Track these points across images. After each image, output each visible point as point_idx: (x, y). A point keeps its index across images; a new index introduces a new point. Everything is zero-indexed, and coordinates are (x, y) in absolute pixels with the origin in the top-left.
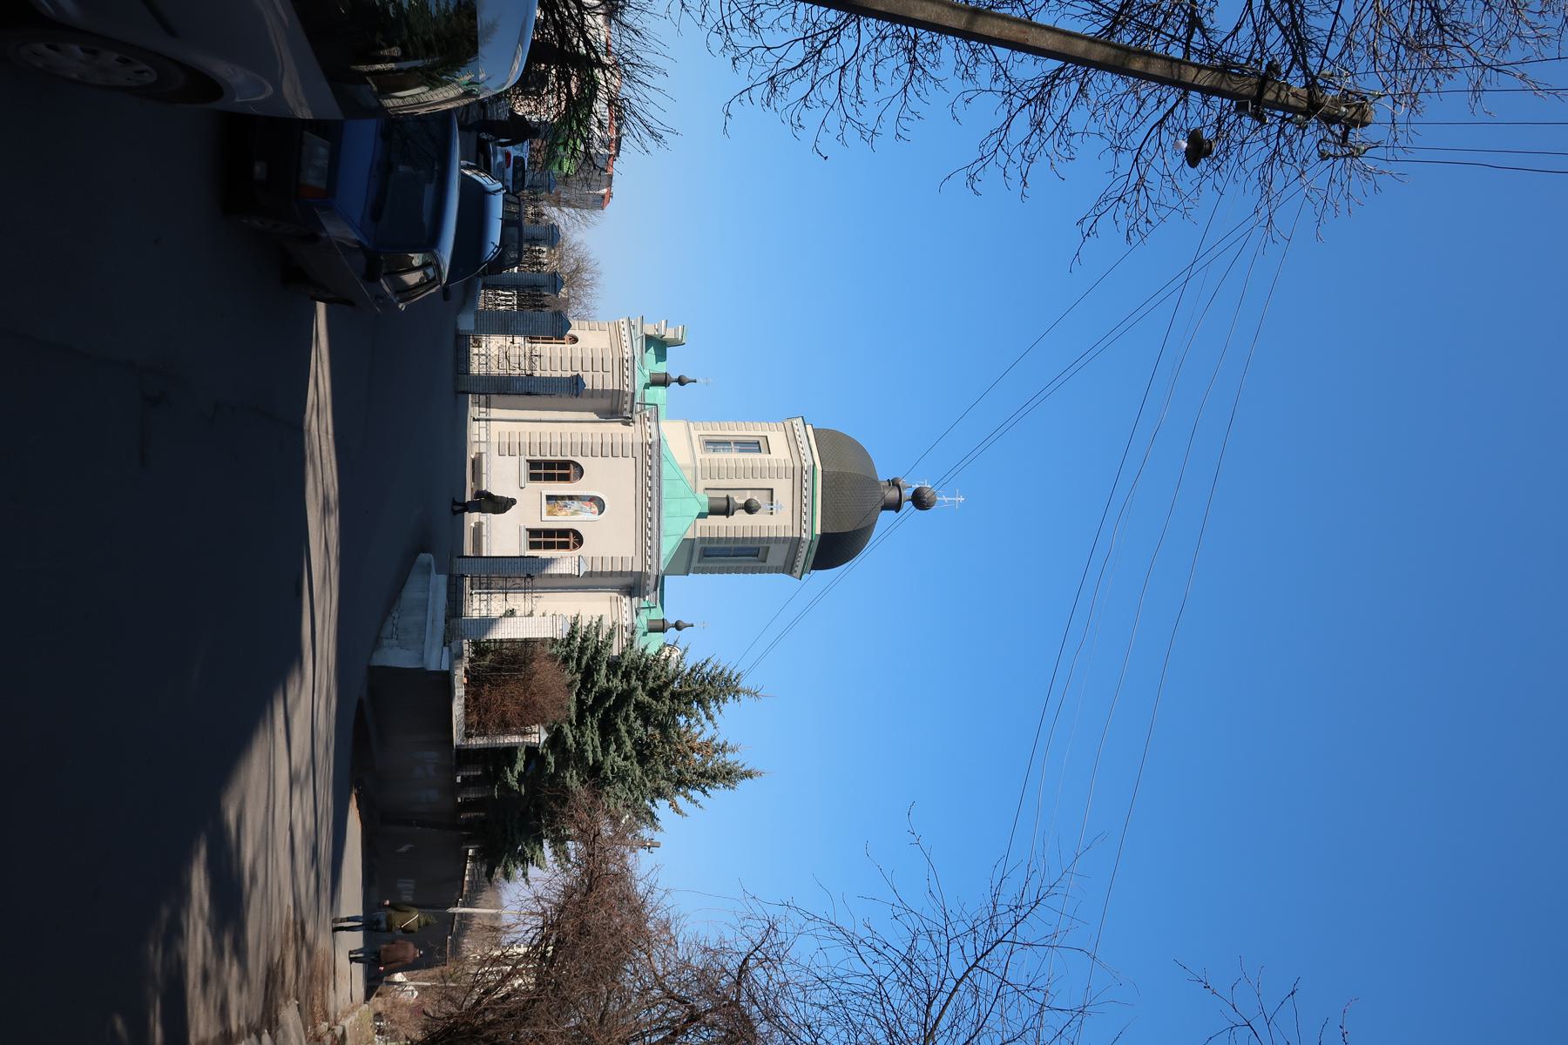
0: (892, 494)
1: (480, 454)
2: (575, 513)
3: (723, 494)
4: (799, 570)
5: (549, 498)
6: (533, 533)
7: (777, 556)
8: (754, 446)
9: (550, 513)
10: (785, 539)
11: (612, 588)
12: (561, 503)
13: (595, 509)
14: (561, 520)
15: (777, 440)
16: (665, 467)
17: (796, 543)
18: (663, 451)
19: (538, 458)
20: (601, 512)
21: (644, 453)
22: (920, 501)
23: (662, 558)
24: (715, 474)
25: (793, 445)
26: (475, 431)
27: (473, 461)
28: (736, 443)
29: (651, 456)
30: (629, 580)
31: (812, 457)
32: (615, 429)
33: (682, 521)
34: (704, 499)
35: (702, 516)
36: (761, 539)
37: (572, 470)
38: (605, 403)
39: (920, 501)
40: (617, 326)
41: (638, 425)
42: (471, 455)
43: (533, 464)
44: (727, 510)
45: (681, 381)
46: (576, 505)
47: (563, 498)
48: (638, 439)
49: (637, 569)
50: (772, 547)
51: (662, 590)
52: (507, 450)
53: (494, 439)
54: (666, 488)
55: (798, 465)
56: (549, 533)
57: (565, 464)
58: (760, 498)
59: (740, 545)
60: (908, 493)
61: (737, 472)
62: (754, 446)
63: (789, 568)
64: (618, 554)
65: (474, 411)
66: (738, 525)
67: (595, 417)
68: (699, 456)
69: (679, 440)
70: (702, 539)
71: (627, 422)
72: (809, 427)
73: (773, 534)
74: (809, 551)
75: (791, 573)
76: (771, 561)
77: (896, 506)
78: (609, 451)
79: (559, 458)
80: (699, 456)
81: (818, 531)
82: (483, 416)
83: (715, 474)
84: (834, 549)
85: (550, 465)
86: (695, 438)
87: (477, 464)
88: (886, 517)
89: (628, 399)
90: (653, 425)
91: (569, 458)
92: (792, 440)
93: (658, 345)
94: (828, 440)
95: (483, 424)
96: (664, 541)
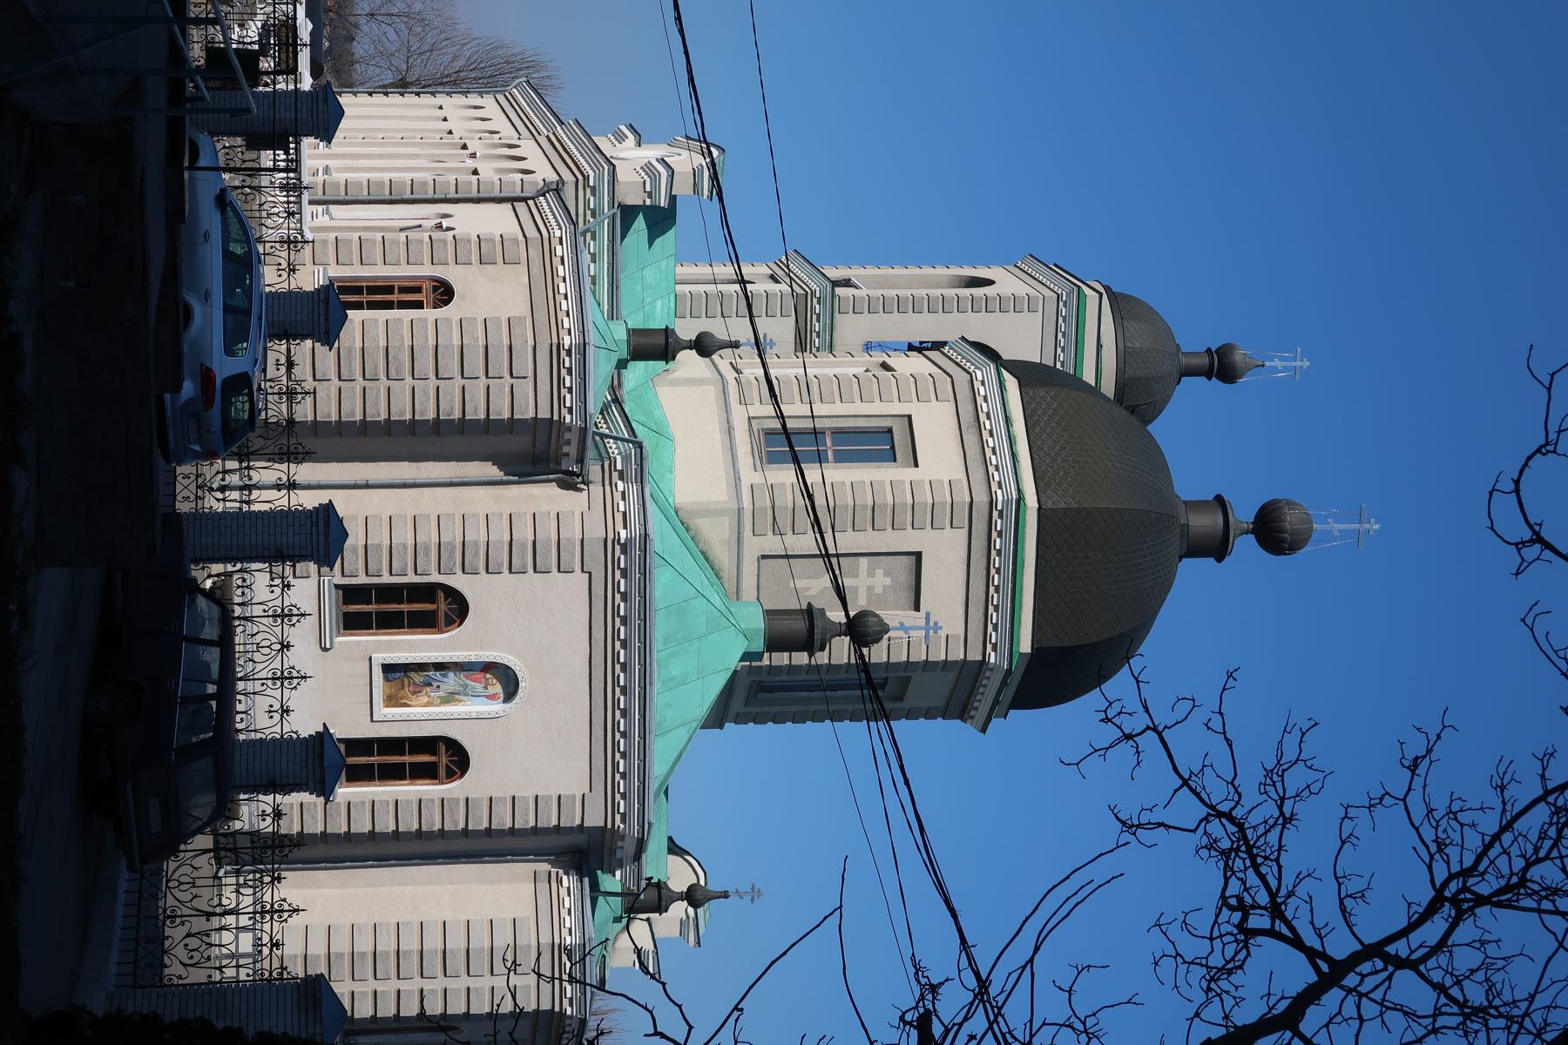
2: (450, 698)
4: (983, 706)
5: (388, 669)
9: (392, 701)
10: (946, 664)
11: (538, 854)
12: (418, 678)
13: (497, 688)
14: (419, 717)
15: (936, 428)
19: (362, 579)
21: (609, 563)
25: (971, 440)
32: (544, 497)
38: (521, 443)
39: (1272, 531)
41: (596, 489)
43: (350, 594)
46: (452, 681)
47: (421, 667)
48: (596, 531)
49: (595, 819)
50: (917, 678)
51: (721, 199)
55: (981, 498)
57: (427, 592)
64: (549, 791)
68: (750, 476)
71: (571, 481)
74: (1004, 683)
76: (911, 700)
77: (1218, 549)
78: (529, 557)
79: (411, 578)
81: (1025, 645)
88: (1192, 572)
89: (573, 436)
90: (633, 491)
92: (971, 426)
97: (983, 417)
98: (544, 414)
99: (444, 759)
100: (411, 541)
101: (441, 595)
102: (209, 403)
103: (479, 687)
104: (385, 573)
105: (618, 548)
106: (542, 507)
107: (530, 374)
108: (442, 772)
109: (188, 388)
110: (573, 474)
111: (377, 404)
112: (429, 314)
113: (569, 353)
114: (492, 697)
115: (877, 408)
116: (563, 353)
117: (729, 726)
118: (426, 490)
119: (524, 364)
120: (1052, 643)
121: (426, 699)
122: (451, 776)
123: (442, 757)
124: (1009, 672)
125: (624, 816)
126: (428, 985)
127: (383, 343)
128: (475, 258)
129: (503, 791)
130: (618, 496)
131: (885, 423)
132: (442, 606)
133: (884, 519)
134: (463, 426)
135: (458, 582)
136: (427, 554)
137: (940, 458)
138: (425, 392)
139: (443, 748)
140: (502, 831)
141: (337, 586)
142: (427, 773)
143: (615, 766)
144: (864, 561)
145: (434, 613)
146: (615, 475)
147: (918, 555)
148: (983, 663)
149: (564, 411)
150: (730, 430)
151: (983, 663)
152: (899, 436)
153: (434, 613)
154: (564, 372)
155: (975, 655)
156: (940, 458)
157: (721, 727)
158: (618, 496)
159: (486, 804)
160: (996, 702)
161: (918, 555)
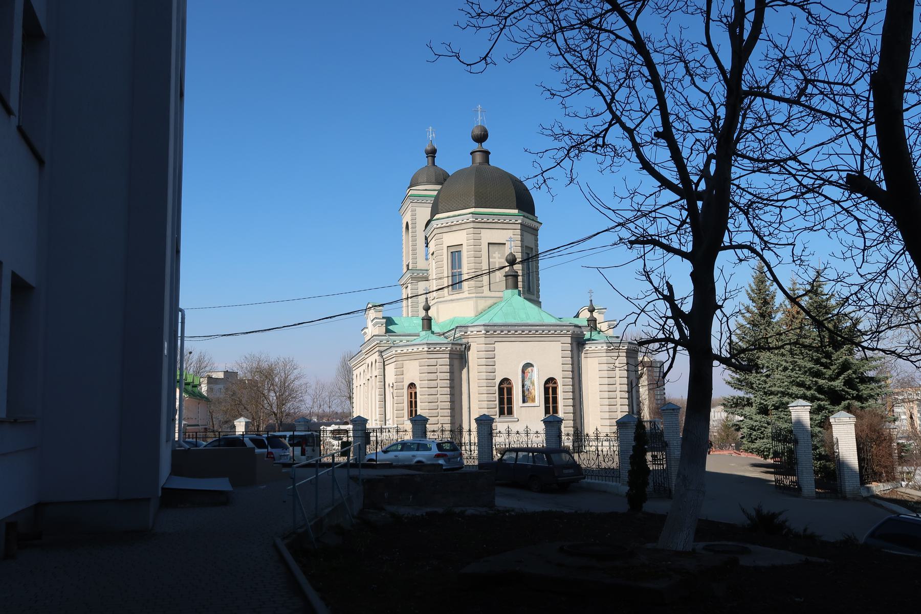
0: (479, 158)
2: (533, 383)
5: (524, 402)
7: (530, 242)
9: (533, 400)
11: (579, 356)
12: (526, 393)
13: (530, 369)
15: (451, 239)
20: (532, 365)
21: (492, 336)
30: (575, 344)
37: (505, 386)
38: (456, 362)
41: (470, 340)
43: (502, 413)
44: (33, 34)
45: (427, 308)
46: (527, 383)
47: (523, 392)
48: (483, 340)
49: (569, 340)
50: (526, 244)
54: (511, 321)
55: (472, 225)
57: (501, 390)
60: (476, 146)
63: (534, 231)
64: (560, 353)
68: (466, 295)
71: (468, 348)
75: (537, 230)
77: (486, 153)
78: (490, 360)
80: (466, 295)
81: (516, 211)
85: (501, 401)
88: (493, 162)
89: (454, 347)
90: (470, 329)
91: (497, 388)
92: (450, 228)
98: (448, 356)
99: (551, 385)
102: (445, 455)
109: (441, 462)
112: (418, 390)
119: (433, 362)
120: (515, 203)
122: (555, 383)
123: (550, 386)
126: (618, 389)
129: (560, 367)
133: (478, 254)
134: (452, 380)
135: (498, 381)
137: (460, 237)
142: (555, 390)
147: (489, 244)
156: (460, 237)
161: (489, 244)
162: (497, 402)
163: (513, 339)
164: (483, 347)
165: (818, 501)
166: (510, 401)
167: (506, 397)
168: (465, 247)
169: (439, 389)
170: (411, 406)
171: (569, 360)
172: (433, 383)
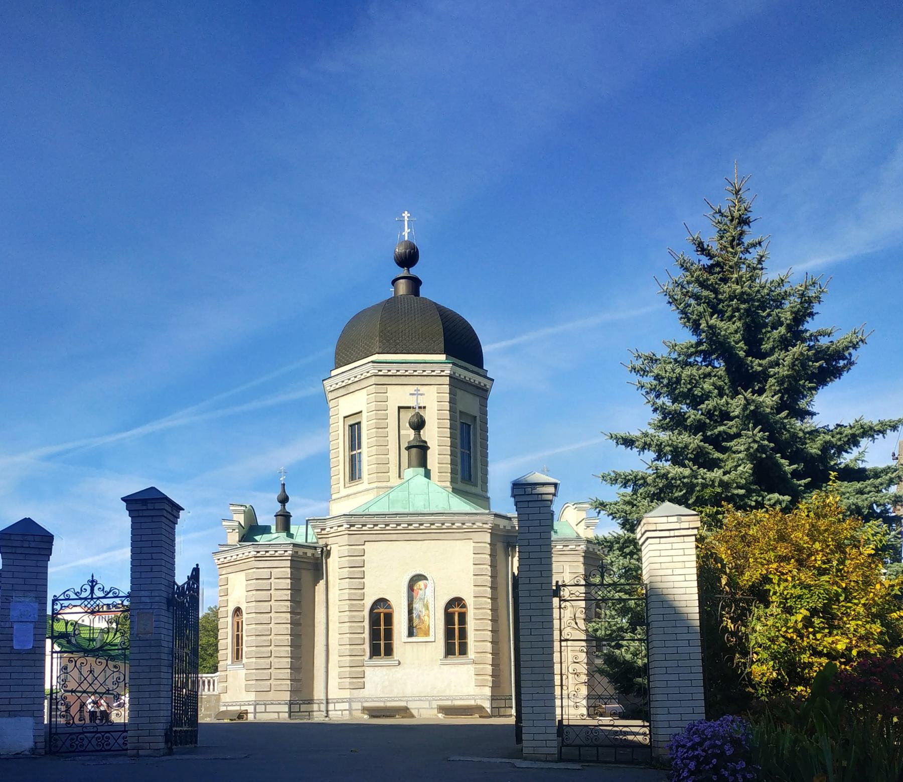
1: (365, 710)
3: (405, 453)
5: (411, 634)
6: (449, 651)
7: (469, 404)
8: (354, 431)
9: (427, 634)
12: (416, 622)
13: (421, 584)
15: (345, 406)
16: (374, 510)
17: (455, 383)
18: (360, 511)
19: (367, 647)
20: (425, 578)
21: (360, 532)
22: (409, 258)
23: (475, 511)
24: (383, 468)
26: (339, 714)
27: (373, 716)
28: (352, 448)
29: (358, 523)
30: (500, 547)
31: (363, 367)
32: (334, 565)
33: (433, 492)
34: (408, 473)
35: (428, 475)
36: (452, 419)
37: (382, 610)
38: (307, 576)
39: (409, 258)
40: (223, 565)
41: (330, 541)
42: (365, 719)
43: (375, 652)
44: (420, 451)
45: (284, 500)
46: (417, 606)
47: (410, 620)
50: (460, 407)
52: (357, 681)
53: (346, 694)
55: (373, 380)
56: (449, 634)
58: (407, 416)
59: (458, 441)
60: (403, 272)
61: (382, 445)
62: (354, 431)
63: (482, 393)
65: (318, 717)
66: (437, 436)
67: (322, 583)
69: (348, 499)
70: (453, 481)
72: (334, 373)
73: (447, 405)
76: (475, 411)
77: (415, 283)
78: (357, 571)
79: (366, 624)
81: (442, 357)
82: (323, 707)
83: (383, 468)
84: (462, 345)
85: (374, 635)
86: (344, 492)
87: (374, 712)
88: (424, 292)
92: (346, 389)
93: (251, 531)
94: (346, 352)
95: (331, 707)
96: (455, 509)
97: (344, 384)
98: (288, 564)
100: (348, 624)
101: (450, 610)
103: (421, 592)
104: (362, 636)
105: (352, 528)
106: (337, 565)
107: (269, 570)
108: (463, 610)
110: (322, 551)
111: (282, 640)
113: (258, 552)
114: (426, 587)
115: (341, 432)
116: (259, 555)
117: (489, 495)
118: (330, 619)
119: (265, 573)
120: (442, 345)
121: (426, 618)
122: (464, 606)
124: (454, 364)
125: (409, 525)
127: (254, 638)
128: (224, 598)
130: (332, 530)
131: (347, 428)
132: (382, 610)
133: (383, 423)
135: (368, 603)
136: (354, 617)
137: (356, 402)
138: (277, 618)
139: (450, 610)
140: (492, 582)
141: (371, 658)
142: (463, 617)
143: (459, 528)
144: (402, 432)
145: (385, 614)
146: (323, 532)
147: (400, 408)
148: (450, 377)
149: (286, 554)
150: (348, 496)
151: (450, 377)
152: (352, 421)
153: (385, 614)
154: (267, 554)
155: (447, 380)
156: (356, 402)
157: (488, 498)
158: (332, 530)
159: (477, 588)
160: (478, 374)
161: (400, 408)
162: (366, 635)
163: (394, 537)
164: (345, 550)
165: (561, 765)
166: (389, 634)
167: (456, 627)
168: (364, 414)
169: (273, 615)
170: (238, 645)
171: (487, 569)
172: (265, 606)
